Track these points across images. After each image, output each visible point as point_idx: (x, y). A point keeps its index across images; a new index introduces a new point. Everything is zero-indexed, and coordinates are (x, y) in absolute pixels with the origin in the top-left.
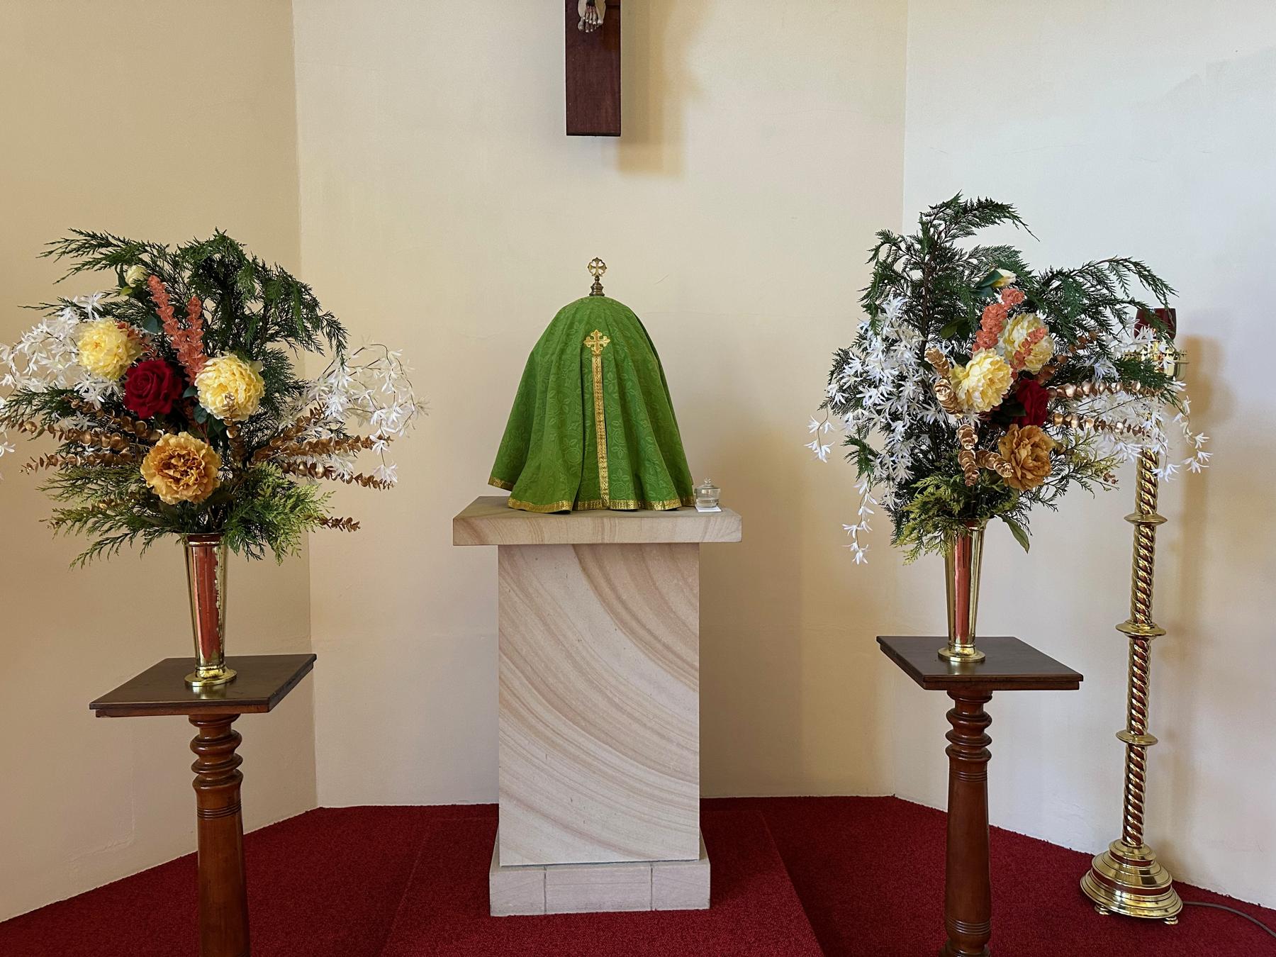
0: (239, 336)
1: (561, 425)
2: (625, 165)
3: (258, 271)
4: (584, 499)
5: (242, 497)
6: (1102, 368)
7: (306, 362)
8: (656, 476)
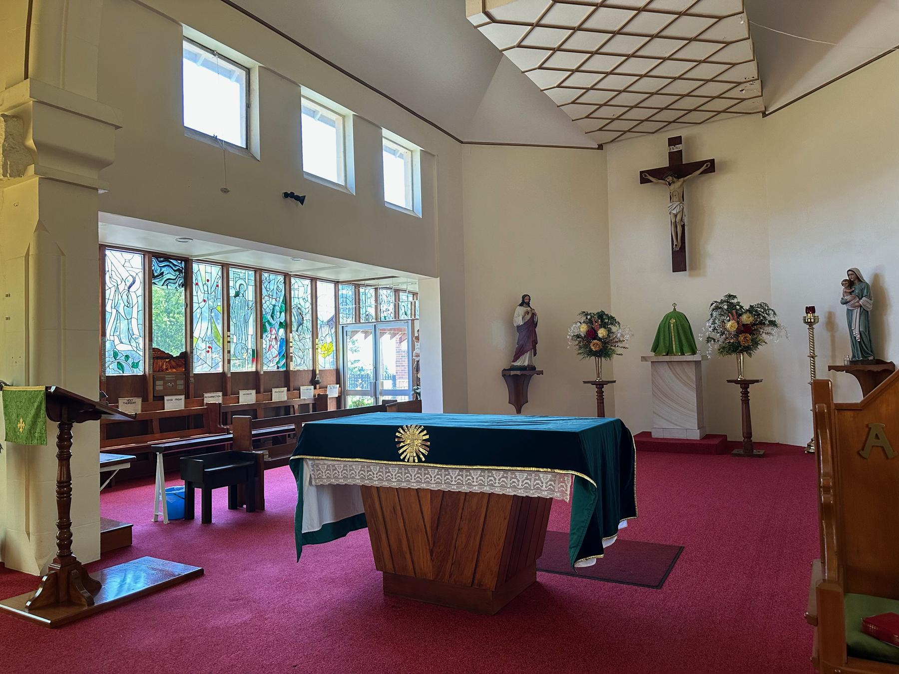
0: (604, 325)
1: (664, 339)
2: (690, 276)
3: (607, 315)
4: (669, 353)
5: (605, 351)
6: (767, 322)
7: (614, 329)
8: (686, 348)
